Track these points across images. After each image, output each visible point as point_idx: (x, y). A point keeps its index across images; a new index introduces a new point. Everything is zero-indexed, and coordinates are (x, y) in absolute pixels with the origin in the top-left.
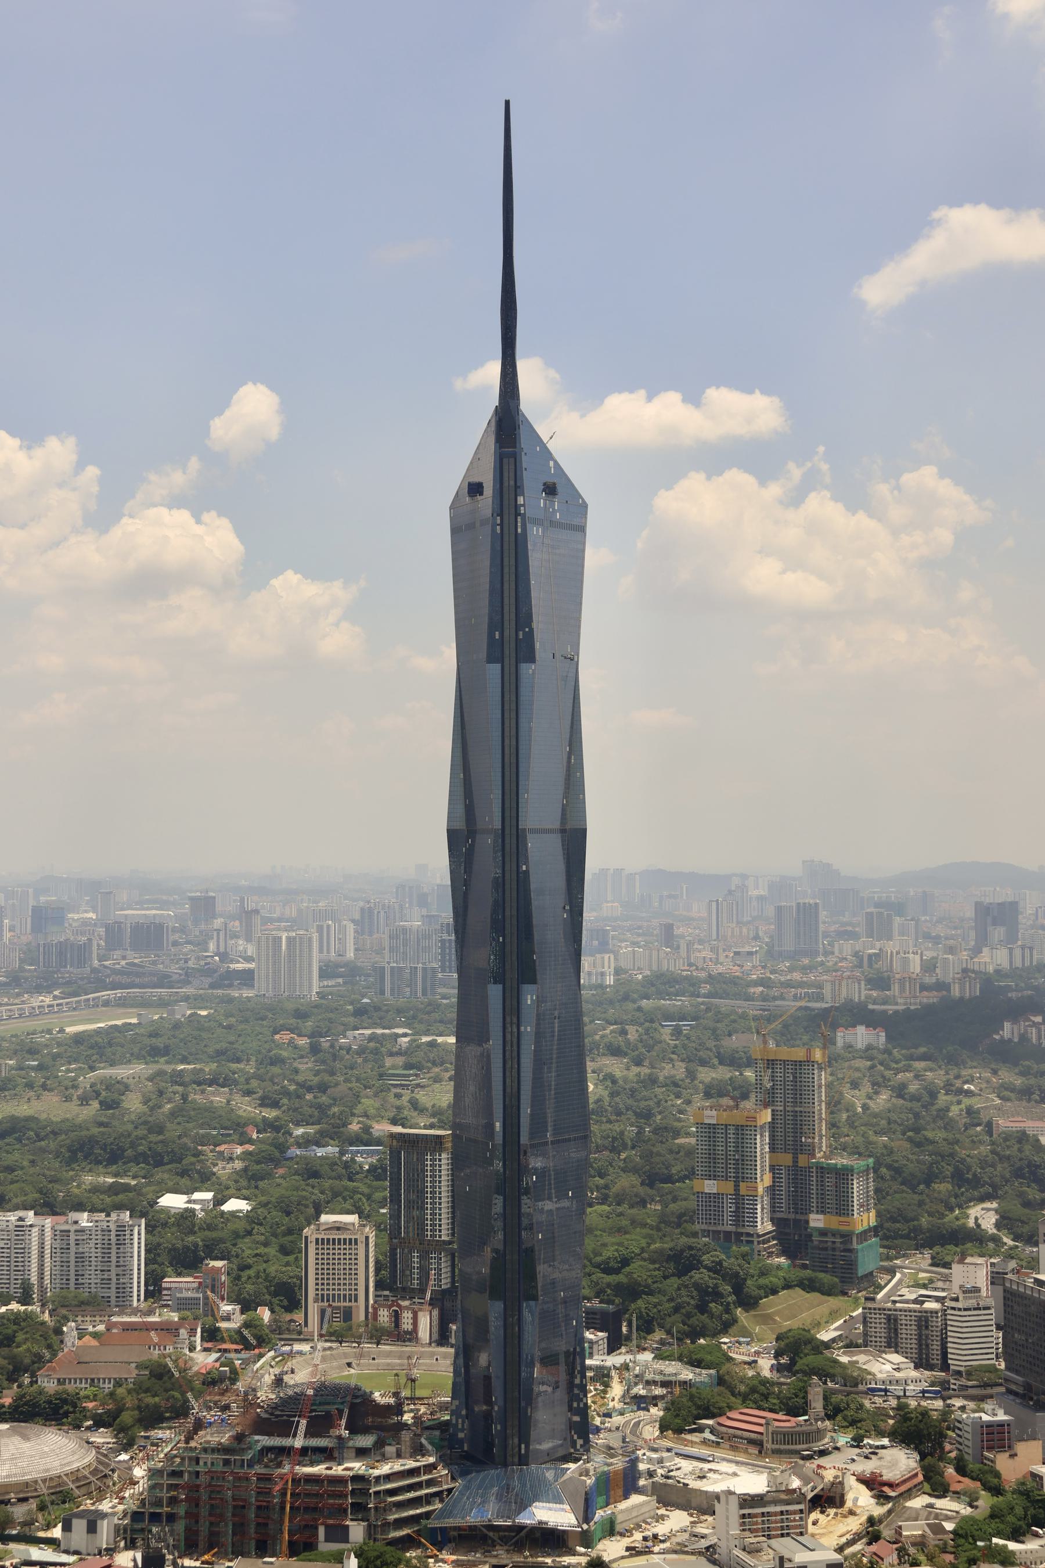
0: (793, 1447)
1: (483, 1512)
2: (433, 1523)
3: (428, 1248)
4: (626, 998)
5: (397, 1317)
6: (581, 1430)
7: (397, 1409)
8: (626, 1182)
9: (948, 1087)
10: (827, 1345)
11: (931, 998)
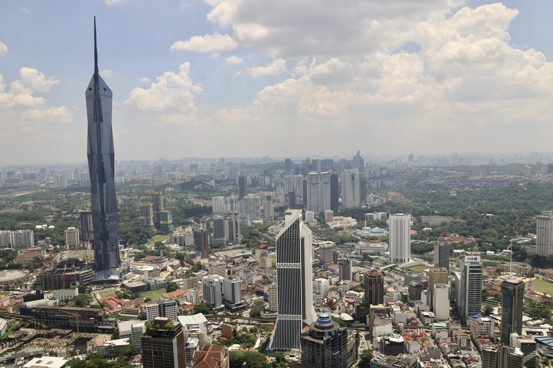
0: (158, 262)
1: (103, 278)
2: (92, 281)
3: (89, 233)
4: (127, 184)
5: (84, 245)
6: (119, 262)
7: (84, 261)
8: (127, 218)
9: (185, 197)
10: (164, 244)
11: (183, 182)
